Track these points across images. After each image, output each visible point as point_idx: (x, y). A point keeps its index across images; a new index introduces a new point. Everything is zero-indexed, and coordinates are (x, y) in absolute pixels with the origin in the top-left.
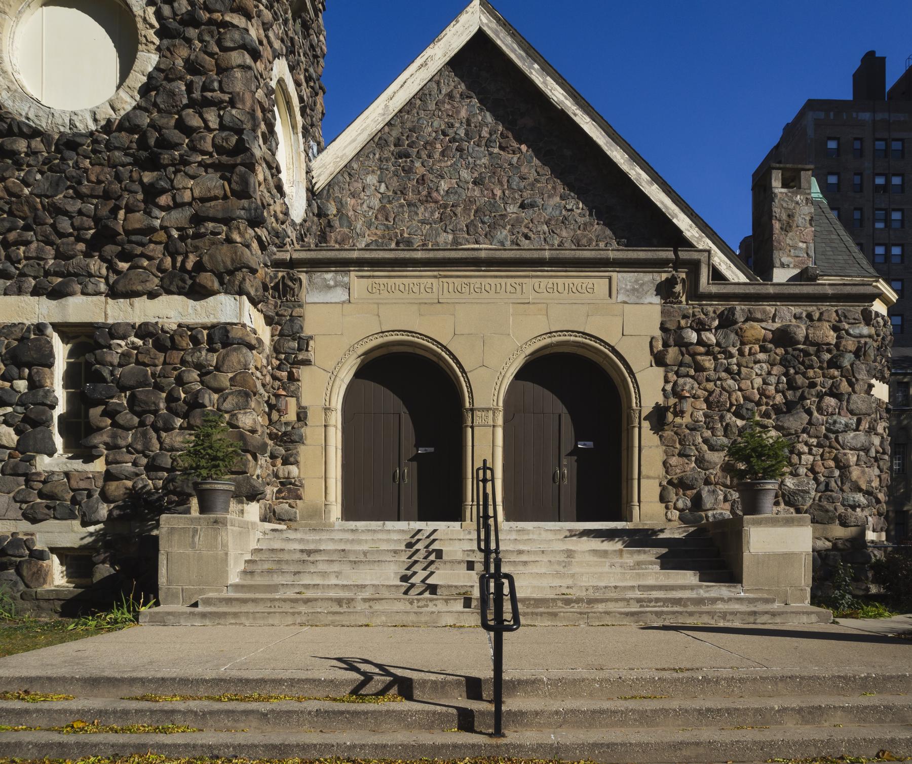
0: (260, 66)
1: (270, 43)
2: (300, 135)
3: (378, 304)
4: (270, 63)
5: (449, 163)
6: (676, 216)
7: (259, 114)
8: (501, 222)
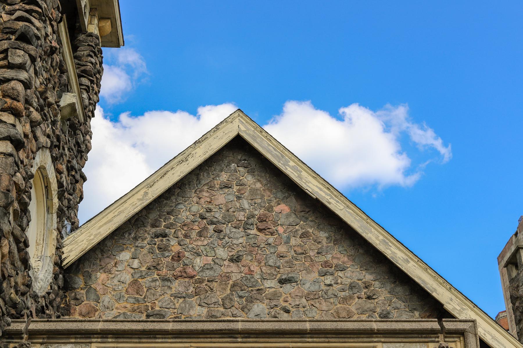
0: (22, 155)
1: (36, 138)
2: (55, 216)
4: (32, 152)
5: (206, 242)
6: (435, 290)
7: (13, 194)
8: (259, 296)
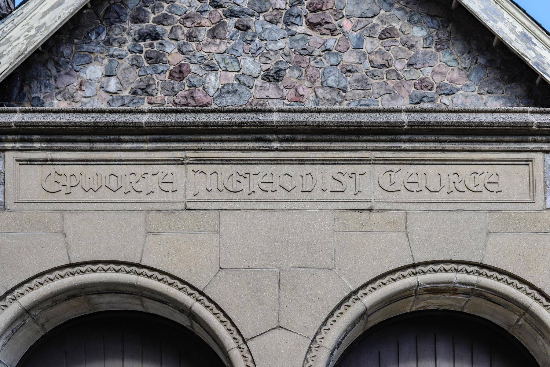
3: (62, 211)
5: (223, 48)
